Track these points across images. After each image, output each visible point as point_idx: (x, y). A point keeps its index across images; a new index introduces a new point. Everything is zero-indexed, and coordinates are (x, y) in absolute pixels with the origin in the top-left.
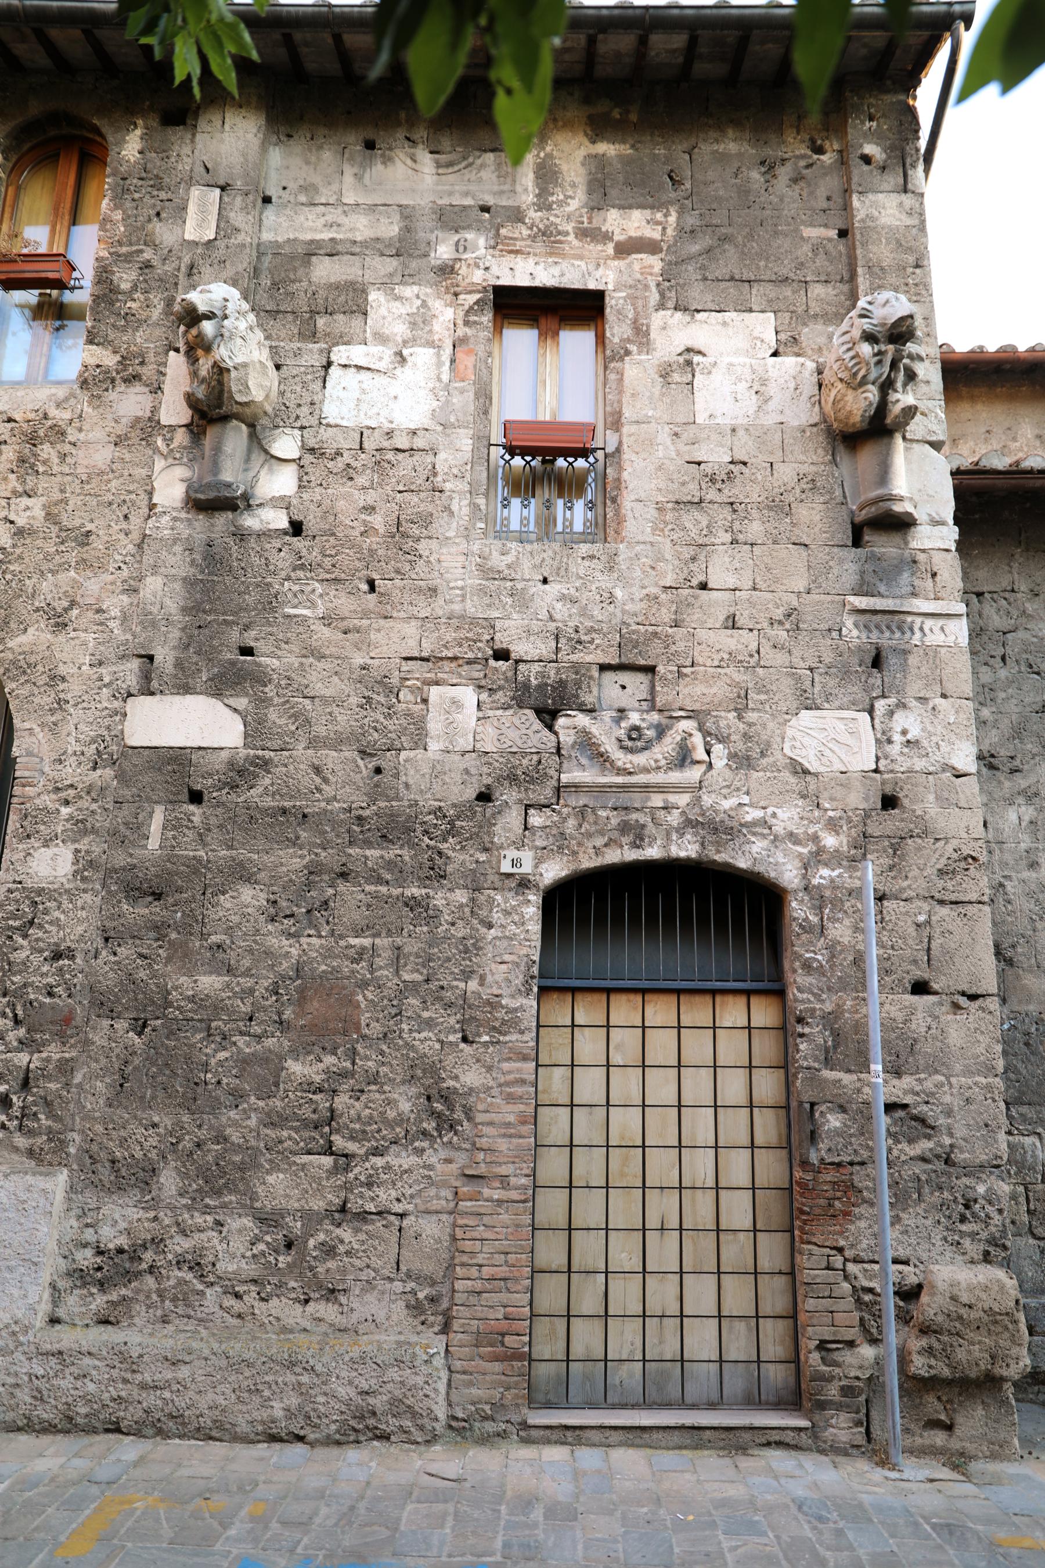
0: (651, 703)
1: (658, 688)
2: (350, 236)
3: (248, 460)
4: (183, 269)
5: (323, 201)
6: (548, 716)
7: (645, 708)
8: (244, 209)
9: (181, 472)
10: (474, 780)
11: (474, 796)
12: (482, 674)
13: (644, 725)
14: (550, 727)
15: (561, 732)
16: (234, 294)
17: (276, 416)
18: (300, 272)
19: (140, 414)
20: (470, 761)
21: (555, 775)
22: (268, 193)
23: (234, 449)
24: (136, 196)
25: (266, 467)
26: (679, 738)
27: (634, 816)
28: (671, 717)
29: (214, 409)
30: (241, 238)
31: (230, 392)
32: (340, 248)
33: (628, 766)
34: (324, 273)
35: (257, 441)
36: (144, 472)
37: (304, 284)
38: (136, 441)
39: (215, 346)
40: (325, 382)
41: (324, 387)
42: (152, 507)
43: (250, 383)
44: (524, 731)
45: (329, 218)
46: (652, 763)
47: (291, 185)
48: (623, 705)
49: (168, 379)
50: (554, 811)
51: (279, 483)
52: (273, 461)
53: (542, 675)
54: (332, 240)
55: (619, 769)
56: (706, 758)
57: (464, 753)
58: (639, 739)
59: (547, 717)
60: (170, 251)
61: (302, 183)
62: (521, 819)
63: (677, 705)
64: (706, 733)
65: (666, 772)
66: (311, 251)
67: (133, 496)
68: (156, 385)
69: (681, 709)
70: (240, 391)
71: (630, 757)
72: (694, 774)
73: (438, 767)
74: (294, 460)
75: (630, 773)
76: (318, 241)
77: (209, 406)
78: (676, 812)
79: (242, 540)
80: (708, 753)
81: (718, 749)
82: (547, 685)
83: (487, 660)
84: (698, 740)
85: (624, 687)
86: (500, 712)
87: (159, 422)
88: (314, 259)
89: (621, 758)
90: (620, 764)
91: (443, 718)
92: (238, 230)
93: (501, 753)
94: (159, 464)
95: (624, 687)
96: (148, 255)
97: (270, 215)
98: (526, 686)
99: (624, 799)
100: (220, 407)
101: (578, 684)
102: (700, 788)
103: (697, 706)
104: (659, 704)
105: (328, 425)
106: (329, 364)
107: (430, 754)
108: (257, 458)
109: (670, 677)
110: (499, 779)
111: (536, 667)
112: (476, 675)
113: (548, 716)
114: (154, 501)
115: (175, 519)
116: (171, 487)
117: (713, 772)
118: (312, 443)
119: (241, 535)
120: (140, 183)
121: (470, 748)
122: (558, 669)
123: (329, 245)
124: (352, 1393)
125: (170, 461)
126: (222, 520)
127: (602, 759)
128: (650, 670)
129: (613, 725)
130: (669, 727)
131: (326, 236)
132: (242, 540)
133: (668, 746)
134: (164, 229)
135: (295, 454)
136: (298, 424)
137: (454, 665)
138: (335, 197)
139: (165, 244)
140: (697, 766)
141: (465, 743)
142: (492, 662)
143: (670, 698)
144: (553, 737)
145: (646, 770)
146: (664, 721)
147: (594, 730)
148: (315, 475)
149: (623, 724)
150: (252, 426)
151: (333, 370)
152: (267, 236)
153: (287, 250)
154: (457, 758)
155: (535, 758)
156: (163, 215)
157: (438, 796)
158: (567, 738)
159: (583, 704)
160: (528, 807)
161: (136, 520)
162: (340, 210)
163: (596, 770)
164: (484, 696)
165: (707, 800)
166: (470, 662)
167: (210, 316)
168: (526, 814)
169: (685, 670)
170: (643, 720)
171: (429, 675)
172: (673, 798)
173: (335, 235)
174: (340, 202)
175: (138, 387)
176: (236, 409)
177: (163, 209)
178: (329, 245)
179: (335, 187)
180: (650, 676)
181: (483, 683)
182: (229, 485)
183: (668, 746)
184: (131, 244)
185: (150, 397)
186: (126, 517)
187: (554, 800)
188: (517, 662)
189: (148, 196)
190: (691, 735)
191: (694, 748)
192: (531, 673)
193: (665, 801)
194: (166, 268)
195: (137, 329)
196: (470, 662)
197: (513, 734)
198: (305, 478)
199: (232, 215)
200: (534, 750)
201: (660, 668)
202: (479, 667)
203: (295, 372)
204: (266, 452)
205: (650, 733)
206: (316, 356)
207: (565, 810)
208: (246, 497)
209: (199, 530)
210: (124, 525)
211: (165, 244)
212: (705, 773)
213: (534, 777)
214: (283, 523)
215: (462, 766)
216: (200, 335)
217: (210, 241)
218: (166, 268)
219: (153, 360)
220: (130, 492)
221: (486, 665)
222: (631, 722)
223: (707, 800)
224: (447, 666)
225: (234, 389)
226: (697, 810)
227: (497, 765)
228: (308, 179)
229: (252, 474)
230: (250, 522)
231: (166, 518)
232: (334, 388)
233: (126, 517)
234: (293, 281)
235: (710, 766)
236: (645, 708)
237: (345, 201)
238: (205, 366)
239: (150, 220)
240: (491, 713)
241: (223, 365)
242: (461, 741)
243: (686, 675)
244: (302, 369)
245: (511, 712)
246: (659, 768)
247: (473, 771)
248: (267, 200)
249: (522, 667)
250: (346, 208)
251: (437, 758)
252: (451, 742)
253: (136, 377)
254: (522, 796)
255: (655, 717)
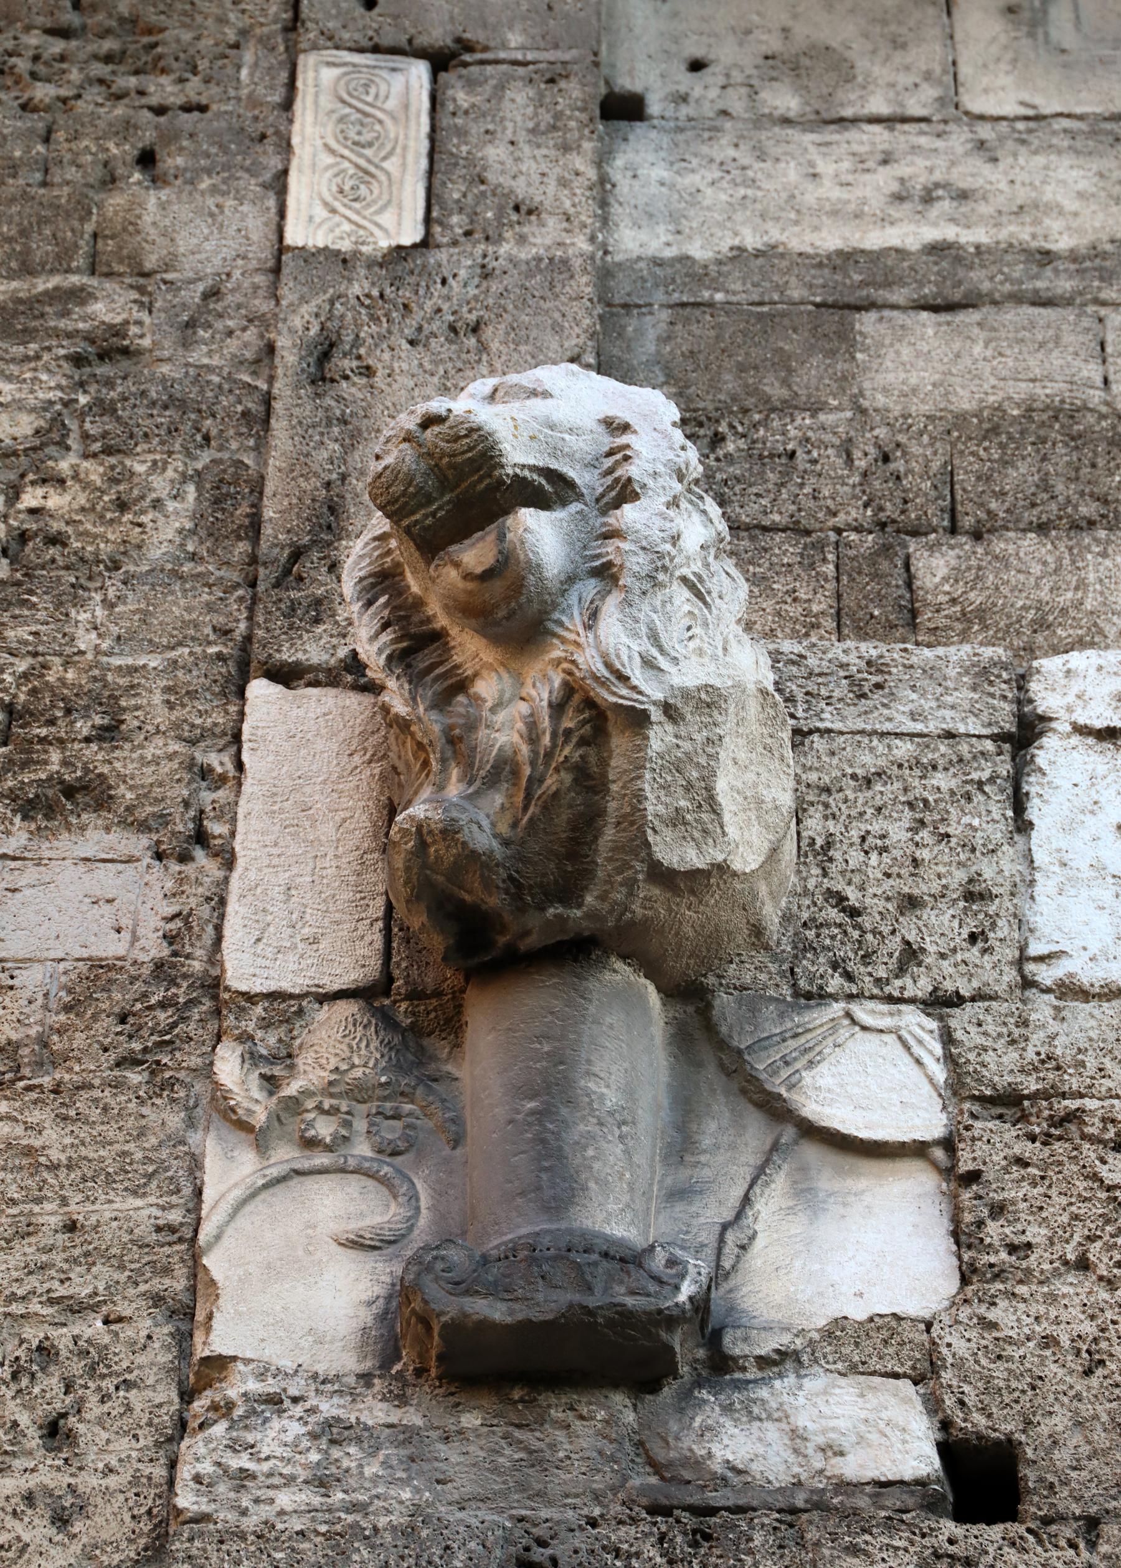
2: (1022, 232)
3: (681, 1146)
4: (289, 356)
5: (878, 105)
8: (549, 130)
9: (340, 1204)
16: (652, 411)
17: (803, 948)
18: (812, 374)
19: (112, 947)
22: (626, 83)
23: (629, 1092)
24: (43, 92)
25: (780, 1182)
29: (523, 910)
30: (544, 237)
31: (634, 819)
32: (979, 279)
34: (923, 377)
35: (722, 1060)
36: (144, 1211)
37: (837, 419)
38: (96, 1066)
39: (575, 620)
40: (1019, 802)
41: (1022, 826)
42: (200, 1374)
43: (721, 786)
45: (916, 170)
47: (725, 53)
49: (251, 801)
51: (861, 1254)
52: (811, 1152)
54: (937, 249)
60: (213, 294)
61: (774, 44)
66: (847, 295)
67: (94, 1328)
68: (183, 825)
70: (677, 820)
74: (918, 1150)
76: (875, 257)
77: (516, 887)
79: (701, 1537)
87: (213, 985)
88: (867, 322)
92: (526, 210)
94: (229, 1168)
96: (109, 306)
97: (643, 163)
100: (568, 891)
105: (1070, 991)
106: (1025, 733)
108: (731, 1144)
114: (221, 1339)
115: (333, 1433)
116: (298, 1276)
118: (1002, 1067)
119: (697, 1511)
120: (57, 46)
123: (932, 270)
125: (285, 1155)
126: (585, 1436)
131: (911, 233)
132: (701, 1537)
134: (183, 211)
135: (927, 1121)
136: (922, 987)
138: (929, 93)
139: (187, 268)
148: (1042, 1216)
150: (689, 997)
151: (1053, 753)
152: (634, 240)
153: (737, 289)
156: (172, 161)
161: (113, 1450)
162: (959, 139)
167: (549, 489)
173: (949, 233)
174: (953, 110)
175: (96, 837)
176: (648, 902)
177: (170, 137)
178: (932, 270)
179: (928, 54)
182: (628, 1259)
184: (27, 270)
185: (162, 878)
186: (55, 1431)
189: (94, 94)
194: (198, 356)
195: (76, 595)
198: (994, 1230)
199: (495, 153)
203: (867, 761)
204: (776, 1109)
206: (964, 696)
208: (707, 1321)
209: (465, 1484)
210: (49, 1475)
211: (187, 268)
214: (915, 1455)
216: (508, 569)
217: (400, 252)
218: (198, 356)
219: (161, 717)
220: (76, 1308)
225: (653, 807)
228: (801, 31)
229: (713, 1212)
230: (741, 1444)
231: (279, 1435)
232: (1069, 828)
233: (55, 1431)
234: (787, 408)
237: (977, 104)
238: (510, 705)
239: (110, 181)
241: (614, 696)
244: (904, 749)
248: (622, 109)
250: (985, 131)
253: (84, 794)
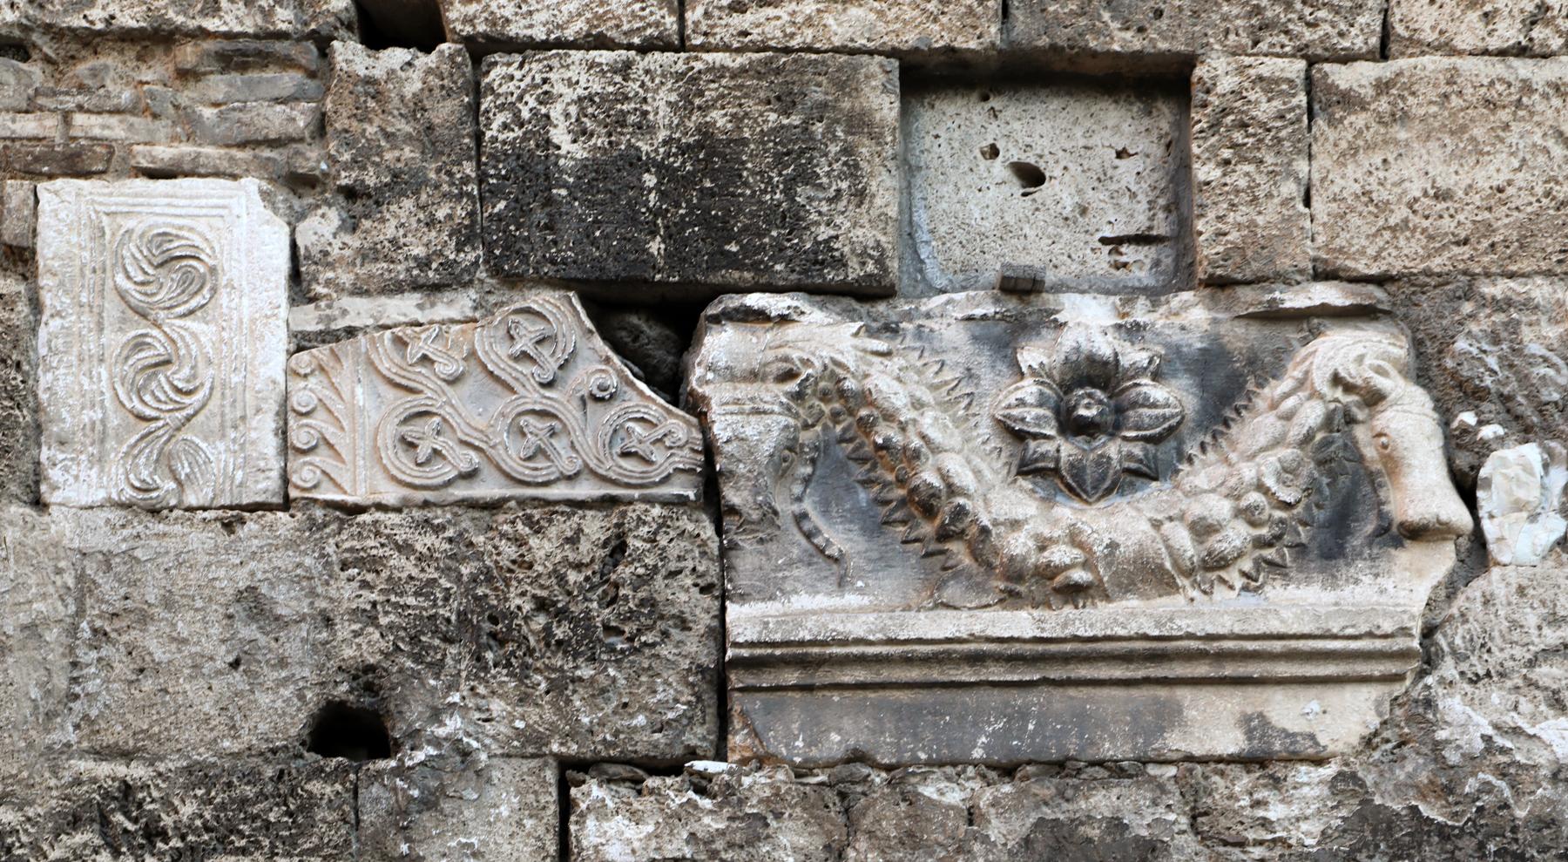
0: (1171, 249)
1: (1205, 171)
6: (653, 322)
7: (1142, 275)
10: (293, 648)
11: (296, 723)
12: (300, 118)
13: (1134, 356)
14: (671, 384)
15: (717, 395)
20: (268, 554)
21: (701, 610)
26: (1312, 414)
27: (1102, 802)
28: (1274, 316)
33: (1060, 554)
44: (534, 398)
46: (1182, 538)
48: (1030, 255)
50: (702, 785)
53: (605, 111)
55: (1015, 573)
56: (1454, 511)
57: (233, 517)
58: (1111, 425)
59: (651, 331)
62: (542, 829)
63: (1304, 252)
64: (1451, 390)
65: (1251, 584)
69: (1324, 274)
71: (1067, 512)
72: (1397, 590)
73: (109, 588)
75: (1074, 593)
78: (1310, 781)
80: (1467, 487)
81: (1514, 467)
82: (635, 162)
83: (323, 44)
84: (1410, 422)
85: (1031, 177)
86: (404, 307)
89: (1024, 520)
90: (1018, 544)
91: (115, 340)
93: (422, 508)
95: (1031, 177)
98: (531, 168)
99: (1046, 719)
101: (796, 158)
102: (1429, 660)
103: (1404, 256)
104: (1208, 251)
107: (60, 524)
109: (1265, 109)
110: (418, 638)
111: (575, 77)
112: (275, 119)
113: (653, 322)
117: (1494, 582)
121: (265, 487)
122: (690, 84)
124: (1339, 822)
127: (929, 526)
128: (1162, 83)
129: (983, 360)
130: (1266, 367)
133: (1262, 453)
137: (153, 72)
140: (1407, 556)
141: (237, 462)
142: (349, 54)
143: (1268, 216)
144: (679, 426)
145: (1151, 575)
146: (1240, 337)
147: (887, 383)
149: (1031, 355)
154: (201, 539)
155: (595, 527)
157: (114, 734)
158: (749, 424)
159: (825, 256)
160: (571, 770)
163: (895, 583)
164: (322, 227)
165: (1466, 718)
166: (239, 56)
168: (566, 807)
169: (1343, 77)
170: (1133, 332)
171: (28, 126)
172: (1289, 712)
180: (1164, 118)
181: (312, 159)
183: (1262, 453)
187: (698, 735)
188: (482, 48)
190: (1374, 399)
191: (1393, 462)
192: (556, 105)
193: (1254, 725)
196: (239, 56)
197: (474, 412)
200: (586, 490)
201: (1218, 72)
202: (289, 80)
205: (1170, 397)
207: (757, 782)
212: (1451, 587)
213: (598, 619)
215: (231, 578)
221: (322, 69)
222: (1069, 340)
223: (1466, 718)
224: (119, 76)
226: (1414, 766)
227: (405, 566)
235: (1477, 554)
236: (1142, 275)
240: (359, 311)
242: (218, 455)
243: (1349, 100)
245: (460, 304)
246: (1217, 563)
247: (287, 601)
249: (502, 73)
251: (101, 540)
252: (165, 461)
254: (540, 715)
255: (1191, 317)
